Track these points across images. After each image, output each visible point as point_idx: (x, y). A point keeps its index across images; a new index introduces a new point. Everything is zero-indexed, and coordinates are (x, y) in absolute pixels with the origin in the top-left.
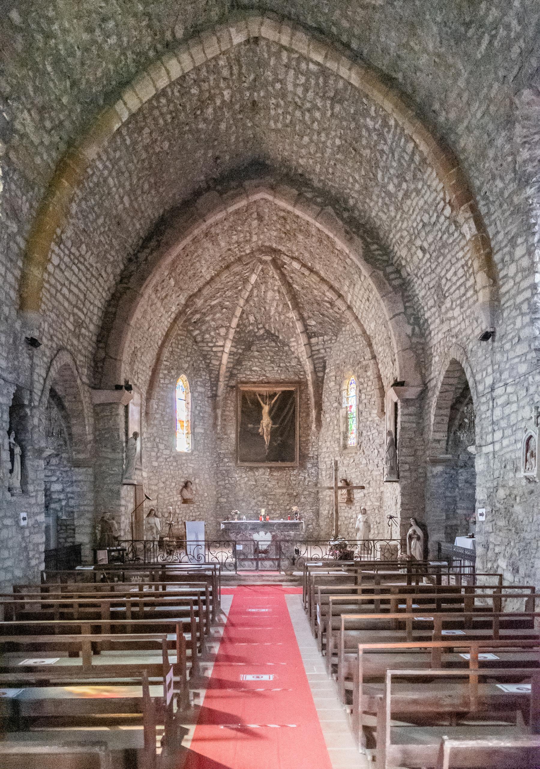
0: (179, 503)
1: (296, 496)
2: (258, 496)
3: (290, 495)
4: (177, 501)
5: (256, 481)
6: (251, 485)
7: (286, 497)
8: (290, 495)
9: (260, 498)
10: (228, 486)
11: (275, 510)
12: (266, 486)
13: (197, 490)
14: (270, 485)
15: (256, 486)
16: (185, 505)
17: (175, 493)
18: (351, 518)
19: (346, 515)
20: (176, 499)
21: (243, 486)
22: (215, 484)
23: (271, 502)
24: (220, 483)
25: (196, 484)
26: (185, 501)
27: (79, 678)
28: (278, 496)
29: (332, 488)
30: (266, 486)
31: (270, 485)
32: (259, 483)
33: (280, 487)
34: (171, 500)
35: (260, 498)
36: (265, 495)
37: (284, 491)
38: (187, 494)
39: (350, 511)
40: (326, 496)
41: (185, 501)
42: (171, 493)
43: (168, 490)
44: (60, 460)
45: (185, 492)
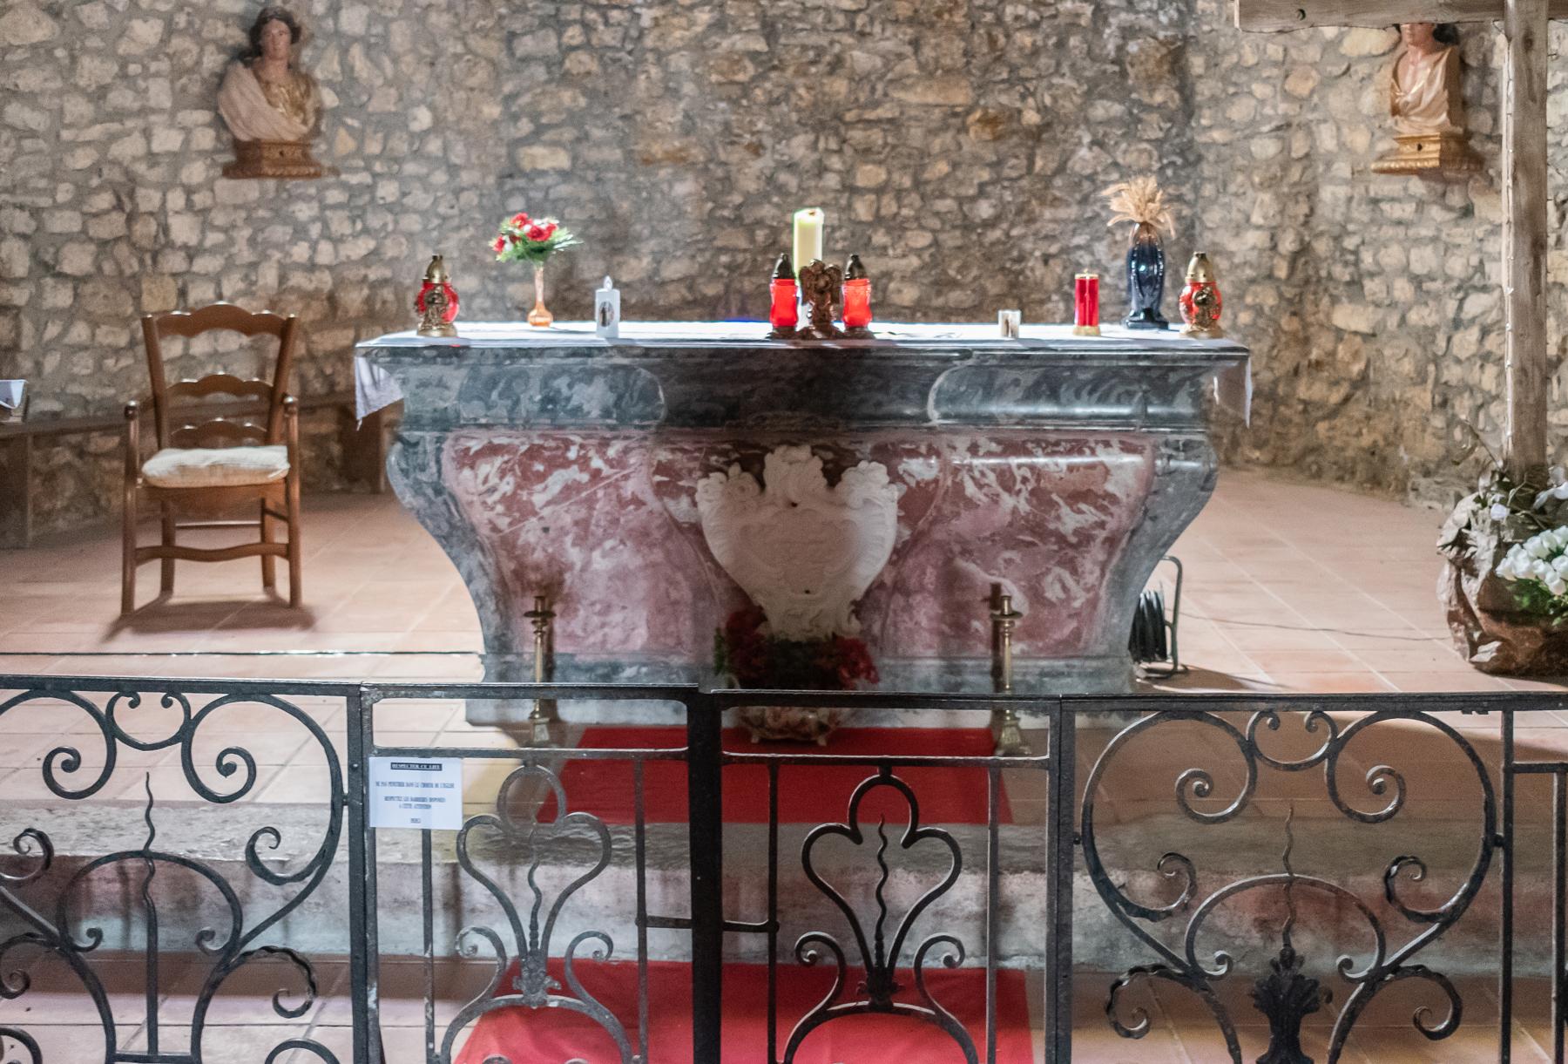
0: (195, 172)
1: (1036, 136)
2: (784, 132)
3: (999, 124)
4: (178, 159)
5: (769, 30)
6: (735, 59)
7: (974, 139)
8: (999, 124)
9: (798, 147)
10: (581, 62)
11: (896, 227)
12: (837, 64)
13: (347, 83)
14: (861, 59)
15: (767, 64)
16: (250, 189)
17: (159, 93)
18: (1465, 288)
19: (1423, 260)
20: (167, 140)
21: (680, 62)
22: (491, 47)
23: (869, 175)
24: (526, 45)
25: (344, 43)
26: (245, 159)
27: (1102, 400)
28: (916, 135)
29: (999, 686)
30: (837, 64)
31: (861, 59)
32: (792, 45)
33: (928, 72)
34: (129, 148)
35: (798, 147)
36: (826, 121)
37: (960, 96)
38: (263, 113)
39: (1462, 234)
40: (1251, 129)
41: (245, 159)
42: (121, 98)
43: (93, 70)
44: (1358, 422)
45: (244, 91)
